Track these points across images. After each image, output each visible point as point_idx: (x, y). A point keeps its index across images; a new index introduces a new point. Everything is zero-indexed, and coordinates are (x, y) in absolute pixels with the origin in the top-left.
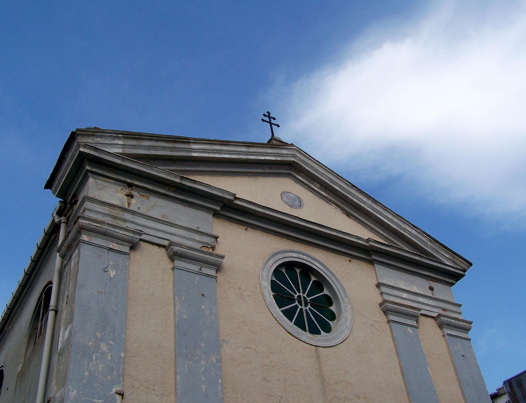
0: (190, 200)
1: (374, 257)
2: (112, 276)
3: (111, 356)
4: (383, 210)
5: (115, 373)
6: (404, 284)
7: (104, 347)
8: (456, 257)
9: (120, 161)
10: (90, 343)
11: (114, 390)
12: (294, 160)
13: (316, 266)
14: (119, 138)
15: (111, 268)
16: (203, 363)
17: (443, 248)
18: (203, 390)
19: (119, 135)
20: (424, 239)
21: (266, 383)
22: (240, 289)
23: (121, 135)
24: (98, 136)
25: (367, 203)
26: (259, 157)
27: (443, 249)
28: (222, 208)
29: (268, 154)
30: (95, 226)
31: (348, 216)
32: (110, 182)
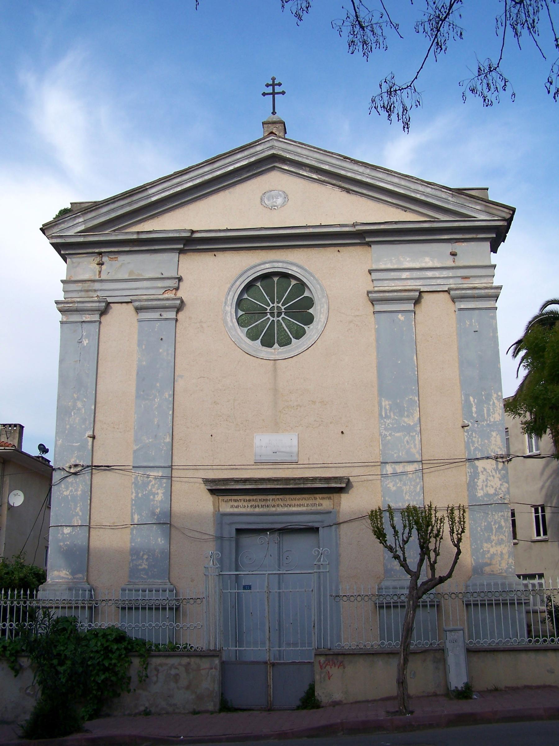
0: (153, 248)
1: (367, 240)
2: (85, 345)
3: (85, 410)
4: (386, 175)
5: (87, 422)
6: (410, 259)
7: (79, 405)
8: (491, 205)
9: (82, 238)
10: (70, 404)
11: (87, 436)
12: (272, 152)
13: (293, 270)
14: (79, 217)
15: (85, 338)
16: (157, 400)
17: (472, 199)
18: (156, 423)
19: (78, 214)
20: (443, 195)
21: (215, 406)
22: (201, 322)
23: (79, 214)
24: (60, 224)
25: (365, 173)
26: (227, 169)
27: (471, 200)
28: (184, 245)
29: (238, 161)
30: (68, 307)
31: (348, 192)
32: (83, 257)
